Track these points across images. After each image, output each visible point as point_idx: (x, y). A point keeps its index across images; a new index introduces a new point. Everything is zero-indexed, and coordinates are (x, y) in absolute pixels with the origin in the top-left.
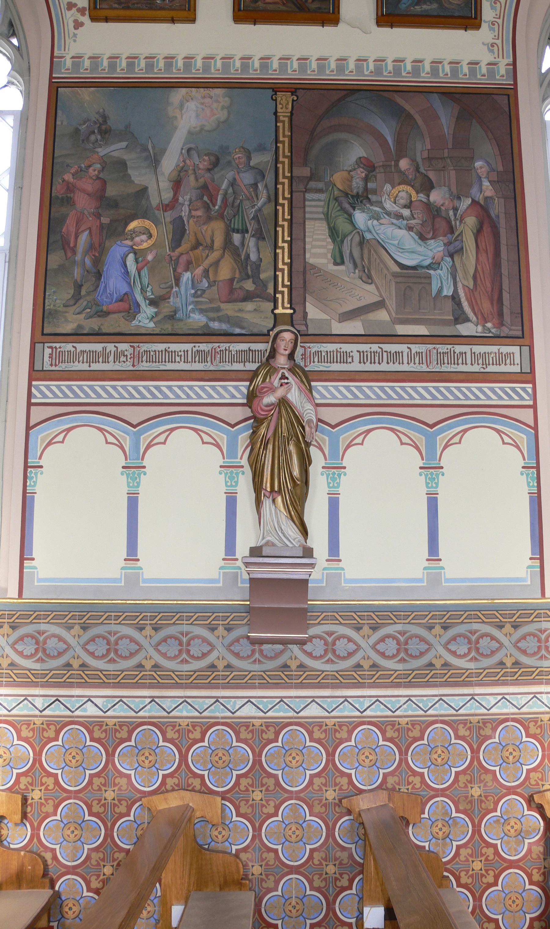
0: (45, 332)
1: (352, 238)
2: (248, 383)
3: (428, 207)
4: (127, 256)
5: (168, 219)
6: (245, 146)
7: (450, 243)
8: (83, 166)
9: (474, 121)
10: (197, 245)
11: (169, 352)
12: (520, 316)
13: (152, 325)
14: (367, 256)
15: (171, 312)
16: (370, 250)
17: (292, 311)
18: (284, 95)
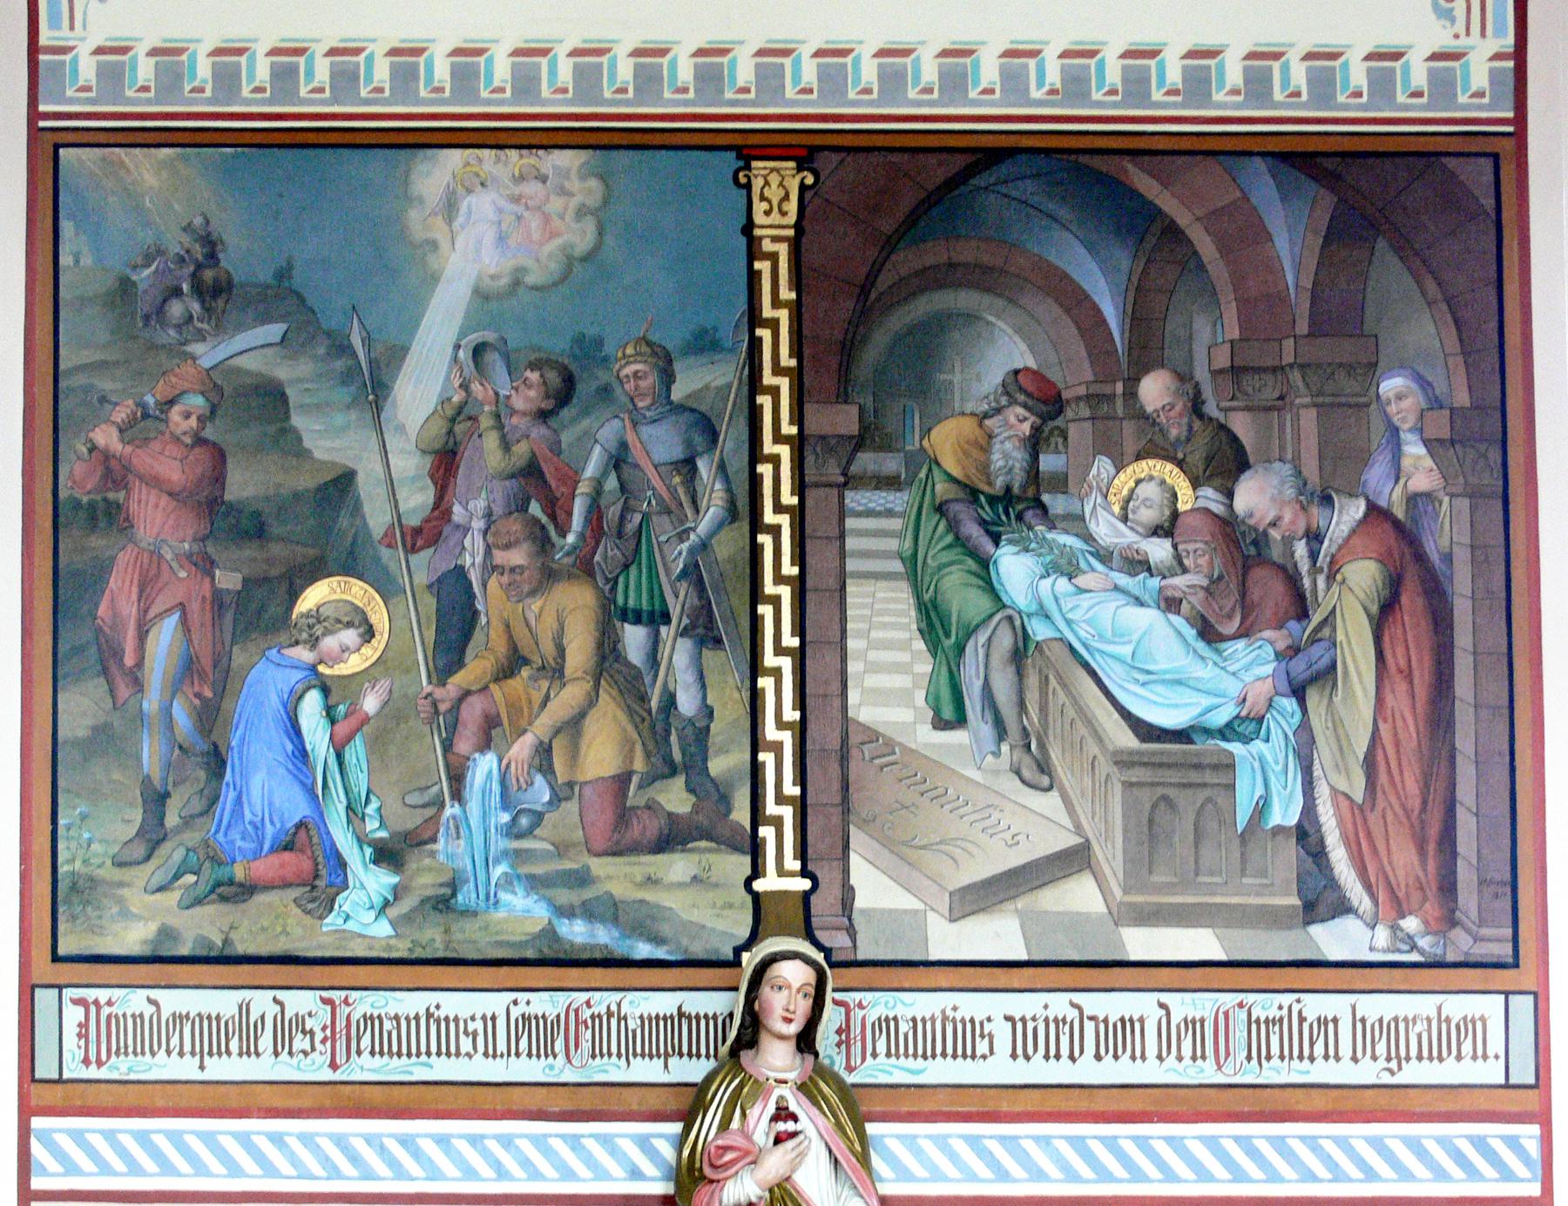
0: (61, 951)
1: (990, 639)
2: (676, 1128)
3: (1228, 528)
4: (300, 698)
5: (421, 578)
6: (655, 337)
7: (1295, 650)
8: (150, 400)
9: (1381, 244)
10: (513, 663)
11: (438, 1021)
12: (1508, 890)
13: (383, 929)
14: (1037, 695)
15: (441, 885)
16: (1047, 678)
17: (806, 884)
18: (772, 170)
